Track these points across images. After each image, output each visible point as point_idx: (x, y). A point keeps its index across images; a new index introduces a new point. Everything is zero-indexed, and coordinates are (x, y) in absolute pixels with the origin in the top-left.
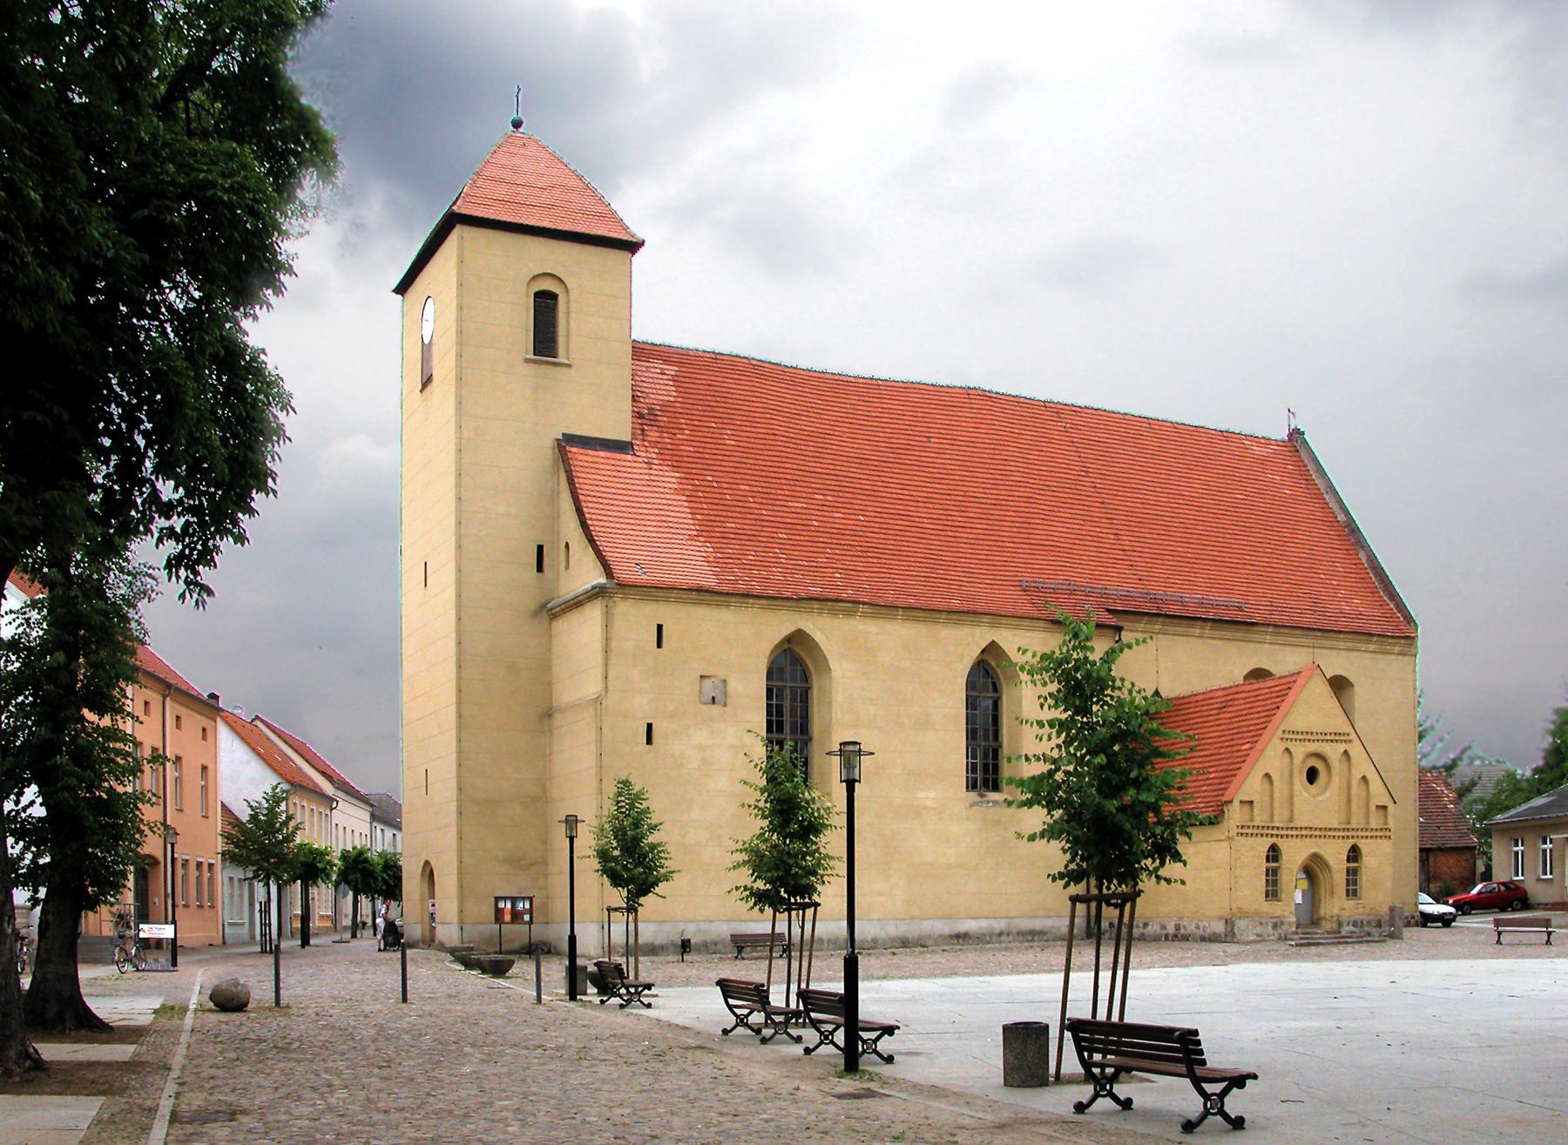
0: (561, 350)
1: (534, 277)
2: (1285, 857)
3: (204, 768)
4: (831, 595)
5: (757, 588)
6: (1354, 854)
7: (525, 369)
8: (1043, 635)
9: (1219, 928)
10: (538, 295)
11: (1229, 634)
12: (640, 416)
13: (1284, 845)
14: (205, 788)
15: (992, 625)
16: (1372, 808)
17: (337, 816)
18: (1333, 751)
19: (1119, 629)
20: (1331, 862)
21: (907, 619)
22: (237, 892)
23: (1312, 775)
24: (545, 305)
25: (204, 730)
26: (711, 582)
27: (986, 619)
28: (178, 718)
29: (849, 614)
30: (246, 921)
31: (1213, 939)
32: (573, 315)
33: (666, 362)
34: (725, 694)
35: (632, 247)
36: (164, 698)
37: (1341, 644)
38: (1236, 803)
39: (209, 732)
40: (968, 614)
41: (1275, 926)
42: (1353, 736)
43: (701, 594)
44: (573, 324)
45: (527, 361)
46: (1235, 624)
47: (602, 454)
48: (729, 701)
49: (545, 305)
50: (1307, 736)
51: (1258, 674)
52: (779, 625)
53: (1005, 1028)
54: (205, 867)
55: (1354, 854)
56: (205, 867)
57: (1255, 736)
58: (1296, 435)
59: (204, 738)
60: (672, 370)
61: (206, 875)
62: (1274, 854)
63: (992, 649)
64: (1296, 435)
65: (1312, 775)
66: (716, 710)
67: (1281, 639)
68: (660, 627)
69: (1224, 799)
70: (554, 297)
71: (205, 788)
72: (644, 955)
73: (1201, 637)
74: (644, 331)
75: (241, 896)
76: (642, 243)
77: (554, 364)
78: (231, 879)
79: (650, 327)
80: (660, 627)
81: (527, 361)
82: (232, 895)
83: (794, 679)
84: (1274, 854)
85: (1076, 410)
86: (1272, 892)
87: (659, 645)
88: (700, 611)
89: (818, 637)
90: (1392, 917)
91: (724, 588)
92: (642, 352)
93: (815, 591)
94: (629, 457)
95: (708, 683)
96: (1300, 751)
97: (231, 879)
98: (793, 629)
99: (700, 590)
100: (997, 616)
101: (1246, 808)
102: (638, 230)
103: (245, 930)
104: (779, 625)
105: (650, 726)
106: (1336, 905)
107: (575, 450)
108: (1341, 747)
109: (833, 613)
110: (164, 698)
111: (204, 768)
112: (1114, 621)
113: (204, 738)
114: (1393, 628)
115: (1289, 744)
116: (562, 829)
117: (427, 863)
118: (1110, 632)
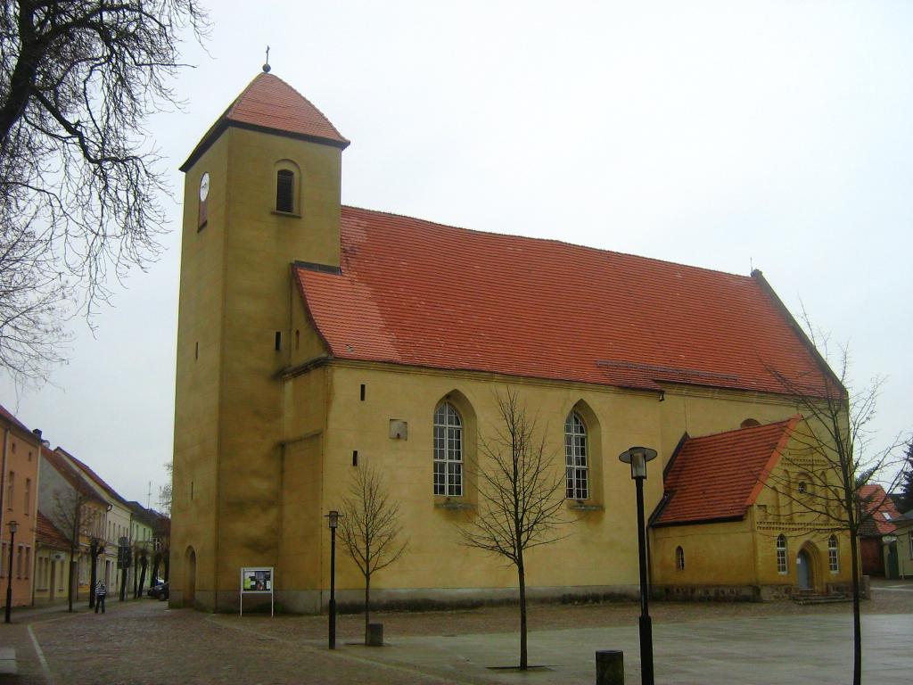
3: (28, 481)
4: (477, 368)
5: (427, 362)
7: (274, 219)
8: (614, 396)
9: (747, 592)
11: (737, 397)
12: (345, 251)
14: (27, 494)
15: (581, 389)
17: (110, 516)
19: (662, 392)
21: (526, 384)
22: (43, 568)
25: (30, 454)
26: (398, 358)
27: (577, 385)
28: (14, 445)
29: (488, 380)
30: (48, 588)
33: (361, 218)
34: (407, 432)
36: (6, 431)
37: (770, 401)
38: (755, 507)
39: (33, 456)
40: (566, 383)
43: (390, 365)
45: (273, 213)
46: (732, 390)
47: (321, 274)
48: (409, 438)
49: (286, 184)
51: (749, 423)
52: (444, 386)
53: (597, 653)
54: (24, 550)
56: (24, 550)
57: (765, 459)
58: (182, 169)
59: (30, 460)
60: (364, 224)
61: (24, 556)
63: (581, 406)
64: (182, 169)
66: (401, 443)
67: (723, 396)
68: (363, 387)
69: (746, 504)
71: (27, 494)
72: (341, 613)
73: (712, 398)
75: (46, 571)
76: (348, 143)
78: (41, 558)
80: (363, 387)
82: (40, 570)
83: (576, 432)
85: (379, 214)
87: (363, 398)
88: (391, 377)
89: (468, 395)
91: (407, 362)
93: (465, 365)
94: (339, 277)
95: (395, 425)
96: (794, 471)
97: (41, 558)
98: (451, 389)
99: (390, 363)
100: (583, 384)
102: (345, 133)
103: (47, 595)
104: (444, 386)
105: (355, 453)
107: (302, 271)
109: (478, 380)
110: (6, 431)
111: (28, 481)
112: (659, 387)
113: (30, 460)
116: (325, 521)
117: (190, 547)
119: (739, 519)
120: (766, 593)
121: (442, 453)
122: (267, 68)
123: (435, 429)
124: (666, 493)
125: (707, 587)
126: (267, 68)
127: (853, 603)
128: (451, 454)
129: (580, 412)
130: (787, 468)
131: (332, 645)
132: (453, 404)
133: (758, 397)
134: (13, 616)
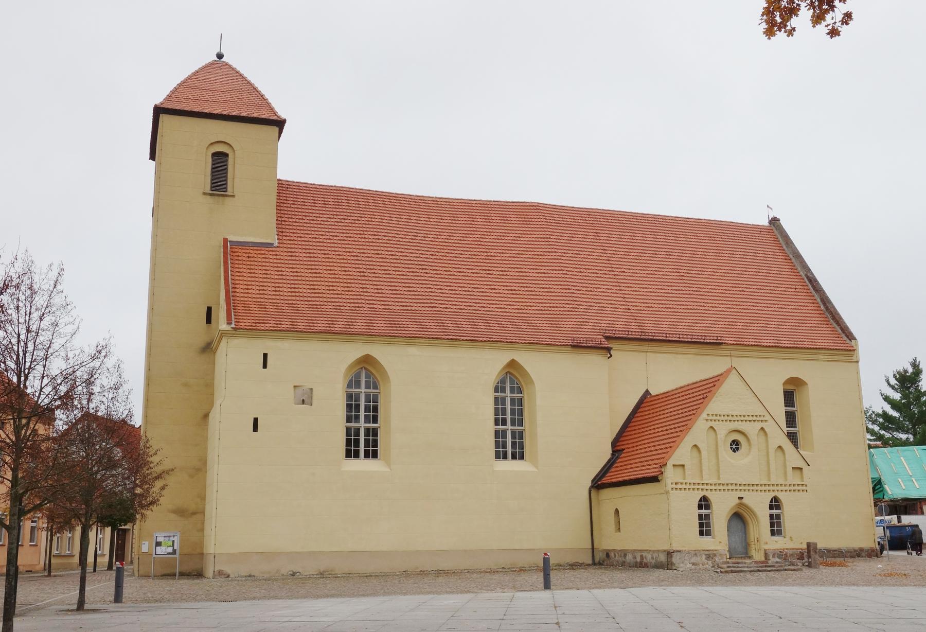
0: (229, 189)
1: (212, 144)
2: (714, 506)
6: (775, 503)
9: (662, 558)
10: (214, 155)
13: (713, 497)
16: (789, 470)
18: (752, 429)
20: (756, 510)
23: (735, 446)
24: (220, 162)
31: (659, 566)
32: (237, 166)
35: (280, 124)
41: (708, 557)
42: (768, 417)
44: (237, 172)
48: (314, 402)
49: (220, 162)
50: (730, 418)
55: (775, 503)
58: (774, 221)
62: (704, 503)
63: (367, 361)
64: (774, 221)
65: (735, 446)
70: (227, 155)
74: (281, 176)
77: (227, 196)
79: (286, 172)
81: (205, 194)
84: (704, 503)
86: (704, 529)
90: (809, 551)
92: (284, 188)
96: (723, 429)
101: (680, 470)
102: (282, 114)
104: (352, 352)
106: (763, 539)
108: (759, 425)
112: (605, 344)
114: (838, 339)
115: (713, 424)
118: (604, 352)
119: (654, 479)
120: (683, 564)
121: (504, 422)
122: (220, 56)
123: (496, 399)
124: (613, 455)
125: (624, 553)
126: (220, 56)
127: (21, 569)
128: (367, 417)
129: (515, 373)
130: (713, 424)
131: (118, 598)
132: (366, 373)
133: (824, 354)
134: (554, 576)
